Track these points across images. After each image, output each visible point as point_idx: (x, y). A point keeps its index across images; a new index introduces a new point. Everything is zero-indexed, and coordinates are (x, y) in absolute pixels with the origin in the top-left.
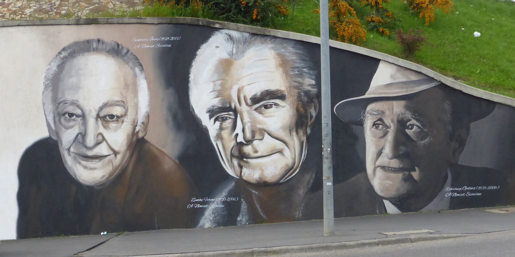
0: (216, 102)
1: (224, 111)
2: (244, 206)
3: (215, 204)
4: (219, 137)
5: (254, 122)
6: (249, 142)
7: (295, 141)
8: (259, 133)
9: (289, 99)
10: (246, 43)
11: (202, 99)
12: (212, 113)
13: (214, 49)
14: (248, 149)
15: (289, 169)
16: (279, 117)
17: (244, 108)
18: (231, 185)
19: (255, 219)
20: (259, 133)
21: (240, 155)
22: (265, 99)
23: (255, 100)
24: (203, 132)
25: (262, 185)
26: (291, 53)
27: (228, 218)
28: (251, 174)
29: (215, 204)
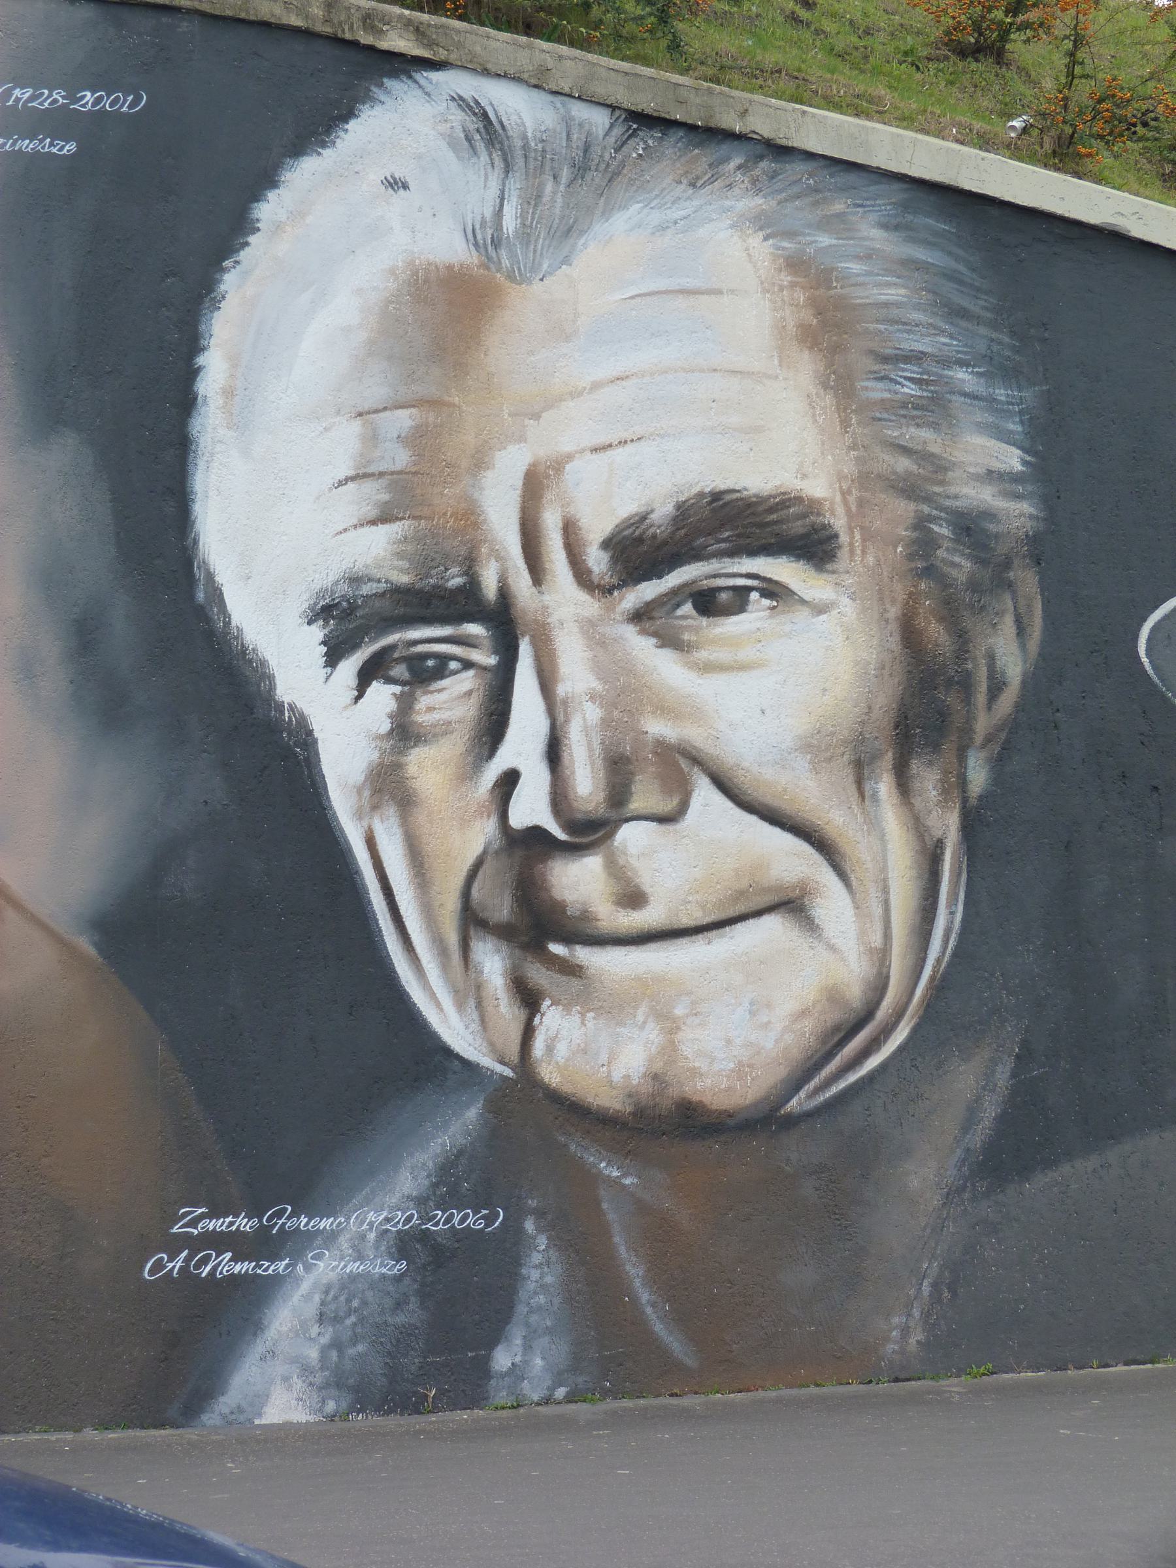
0: (374, 552)
1: (424, 615)
2: (541, 1272)
3: (340, 1260)
4: (388, 785)
5: (624, 695)
6: (588, 832)
7: (885, 838)
8: (656, 771)
9: (857, 560)
10: (591, 177)
11: (279, 522)
12: (346, 621)
13: (353, 222)
14: (578, 881)
15: (849, 1027)
16: (789, 674)
17: (562, 604)
18: (460, 1124)
19: (615, 1363)
20: (656, 771)
21: (534, 927)
22: (702, 552)
23: (639, 553)
24: (281, 755)
25: (669, 1125)
26: (877, 262)
27: (429, 1353)
28: (594, 1050)
29: (340, 1260)
